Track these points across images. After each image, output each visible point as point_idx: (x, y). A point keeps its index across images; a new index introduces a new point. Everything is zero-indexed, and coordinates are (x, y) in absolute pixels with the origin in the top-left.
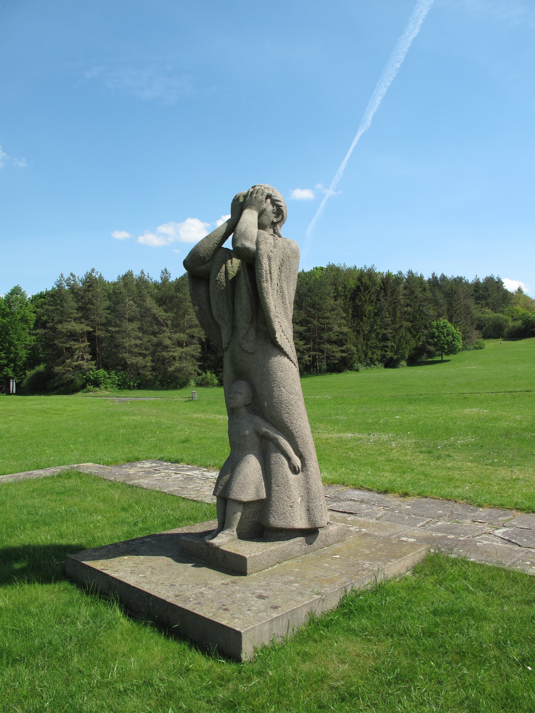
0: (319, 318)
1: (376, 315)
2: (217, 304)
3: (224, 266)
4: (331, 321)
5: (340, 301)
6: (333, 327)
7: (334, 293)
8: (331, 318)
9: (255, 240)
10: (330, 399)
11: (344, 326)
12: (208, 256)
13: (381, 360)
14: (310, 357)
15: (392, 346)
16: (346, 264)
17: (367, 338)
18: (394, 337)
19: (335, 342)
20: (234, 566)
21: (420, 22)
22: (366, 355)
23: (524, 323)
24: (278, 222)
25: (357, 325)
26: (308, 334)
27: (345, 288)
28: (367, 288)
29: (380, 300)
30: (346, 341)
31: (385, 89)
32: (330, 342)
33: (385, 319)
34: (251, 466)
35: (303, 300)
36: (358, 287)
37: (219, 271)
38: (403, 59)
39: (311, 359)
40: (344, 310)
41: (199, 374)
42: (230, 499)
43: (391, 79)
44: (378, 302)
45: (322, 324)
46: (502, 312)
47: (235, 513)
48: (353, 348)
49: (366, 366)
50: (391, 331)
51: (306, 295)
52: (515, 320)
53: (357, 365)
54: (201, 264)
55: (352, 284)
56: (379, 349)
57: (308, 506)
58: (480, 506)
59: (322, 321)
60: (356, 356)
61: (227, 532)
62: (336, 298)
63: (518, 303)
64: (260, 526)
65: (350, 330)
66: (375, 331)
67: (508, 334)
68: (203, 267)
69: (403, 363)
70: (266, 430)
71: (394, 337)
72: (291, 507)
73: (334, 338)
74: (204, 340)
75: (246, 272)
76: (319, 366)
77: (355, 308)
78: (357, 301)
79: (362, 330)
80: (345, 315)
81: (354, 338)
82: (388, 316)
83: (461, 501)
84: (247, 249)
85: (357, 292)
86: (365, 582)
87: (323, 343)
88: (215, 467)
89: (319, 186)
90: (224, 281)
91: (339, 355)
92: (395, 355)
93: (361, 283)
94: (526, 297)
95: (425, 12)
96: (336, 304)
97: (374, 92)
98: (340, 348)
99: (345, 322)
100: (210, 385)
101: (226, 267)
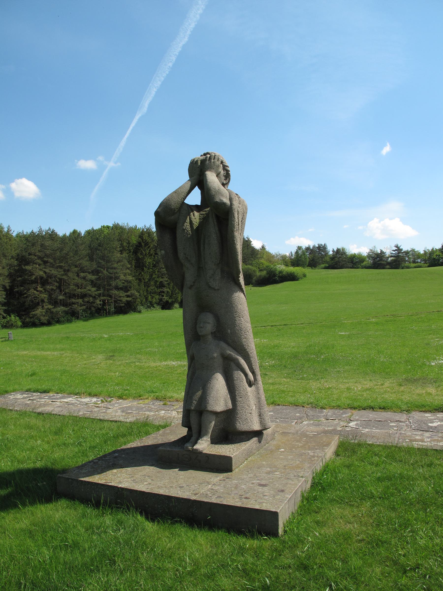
0: (108, 268)
1: (154, 266)
2: (184, 249)
3: (188, 217)
4: (118, 271)
5: (125, 255)
6: (120, 276)
7: (120, 247)
8: (118, 269)
9: (228, 197)
10: (132, 336)
11: (129, 275)
12: (177, 208)
13: (159, 303)
14: (100, 301)
15: (168, 292)
16: (12, 228)
17: (147, 285)
18: (169, 284)
19: (121, 289)
20: (222, 466)
21: (189, 33)
22: (147, 299)
23: (267, 273)
24: (226, 184)
25: (139, 275)
26: (99, 282)
27: (129, 243)
28: (147, 244)
29: (157, 254)
30: (130, 287)
31: (159, 83)
32: (117, 288)
33: (162, 269)
34: (219, 383)
35: (94, 253)
36: (140, 243)
37: (185, 221)
38: (174, 60)
39: (101, 302)
40: (129, 262)
41: (4, 318)
42: (208, 411)
43: (165, 75)
44: (156, 256)
45: (110, 273)
46: (251, 264)
47: (211, 422)
48: (136, 293)
49: (146, 308)
50: (167, 279)
51: (96, 249)
52: (261, 270)
53: (140, 308)
54: (169, 215)
55: (134, 240)
56: (157, 294)
57: (260, 412)
58: (322, 408)
59: (111, 271)
60: (139, 300)
61: (205, 438)
62: (121, 252)
63: (262, 257)
64: (229, 433)
65: (133, 278)
66: (154, 279)
67: (256, 281)
68: (173, 217)
69: (177, 305)
70: (230, 353)
71: (169, 284)
72: (250, 413)
73: (120, 285)
74: (8, 288)
75: (216, 223)
76: (108, 308)
77: (138, 260)
78: (139, 254)
79: (143, 279)
80: (129, 266)
81: (137, 286)
82: (163, 267)
83: (307, 406)
84: (224, 204)
85: (139, 247)
86: (319, 467)
87: (111, 289)
88: (86, 394)
89: (101, 158)
90: (190, 229)
91: (125, 299)
92: (170, 299)
93: (142, 240)
94: (268, 253)
95: (193, 25)
96: (122, 257)
97: (150, 85)
98: (126, 294)
99: (130, 272)
100: (14, 326)
101: (190, 218)
